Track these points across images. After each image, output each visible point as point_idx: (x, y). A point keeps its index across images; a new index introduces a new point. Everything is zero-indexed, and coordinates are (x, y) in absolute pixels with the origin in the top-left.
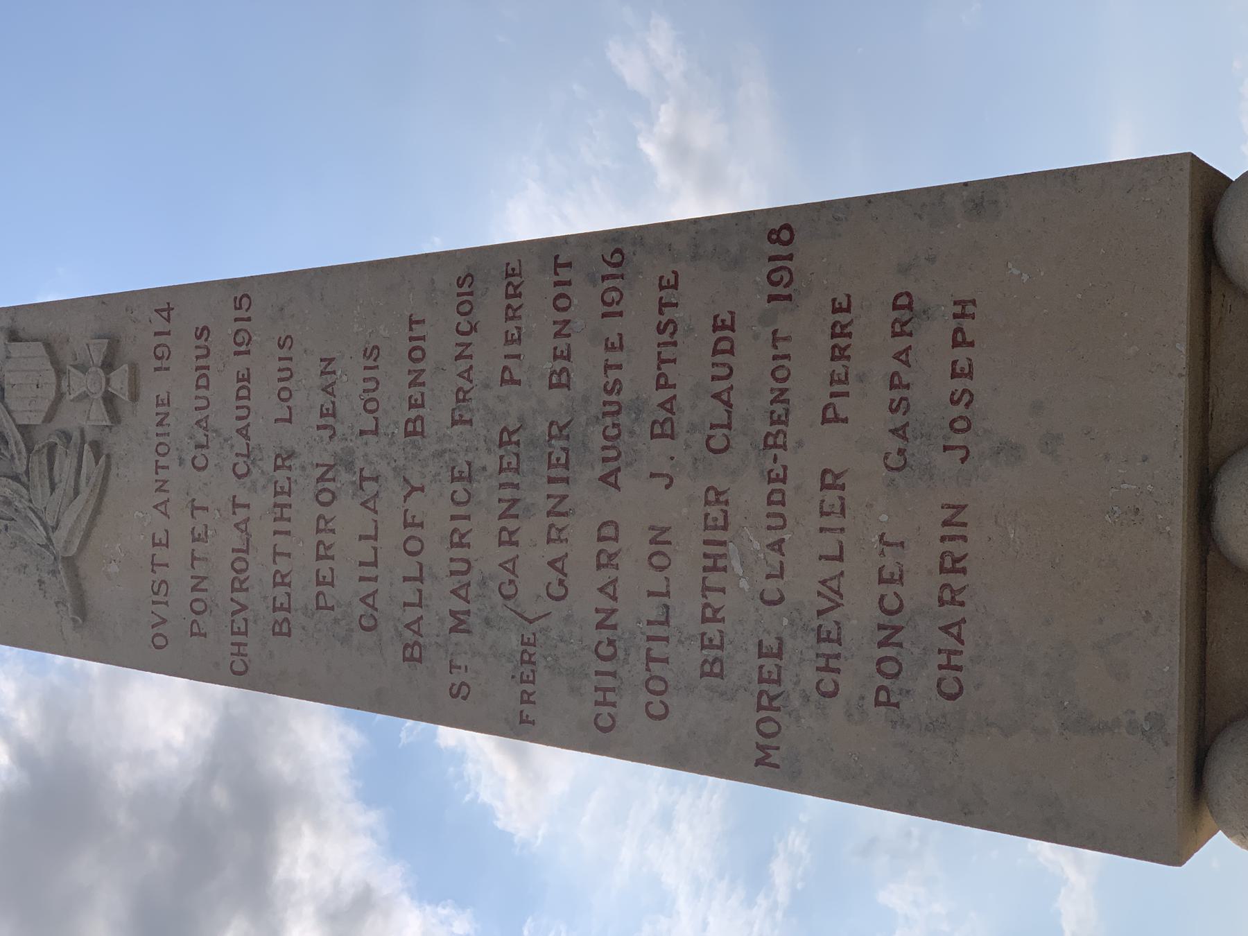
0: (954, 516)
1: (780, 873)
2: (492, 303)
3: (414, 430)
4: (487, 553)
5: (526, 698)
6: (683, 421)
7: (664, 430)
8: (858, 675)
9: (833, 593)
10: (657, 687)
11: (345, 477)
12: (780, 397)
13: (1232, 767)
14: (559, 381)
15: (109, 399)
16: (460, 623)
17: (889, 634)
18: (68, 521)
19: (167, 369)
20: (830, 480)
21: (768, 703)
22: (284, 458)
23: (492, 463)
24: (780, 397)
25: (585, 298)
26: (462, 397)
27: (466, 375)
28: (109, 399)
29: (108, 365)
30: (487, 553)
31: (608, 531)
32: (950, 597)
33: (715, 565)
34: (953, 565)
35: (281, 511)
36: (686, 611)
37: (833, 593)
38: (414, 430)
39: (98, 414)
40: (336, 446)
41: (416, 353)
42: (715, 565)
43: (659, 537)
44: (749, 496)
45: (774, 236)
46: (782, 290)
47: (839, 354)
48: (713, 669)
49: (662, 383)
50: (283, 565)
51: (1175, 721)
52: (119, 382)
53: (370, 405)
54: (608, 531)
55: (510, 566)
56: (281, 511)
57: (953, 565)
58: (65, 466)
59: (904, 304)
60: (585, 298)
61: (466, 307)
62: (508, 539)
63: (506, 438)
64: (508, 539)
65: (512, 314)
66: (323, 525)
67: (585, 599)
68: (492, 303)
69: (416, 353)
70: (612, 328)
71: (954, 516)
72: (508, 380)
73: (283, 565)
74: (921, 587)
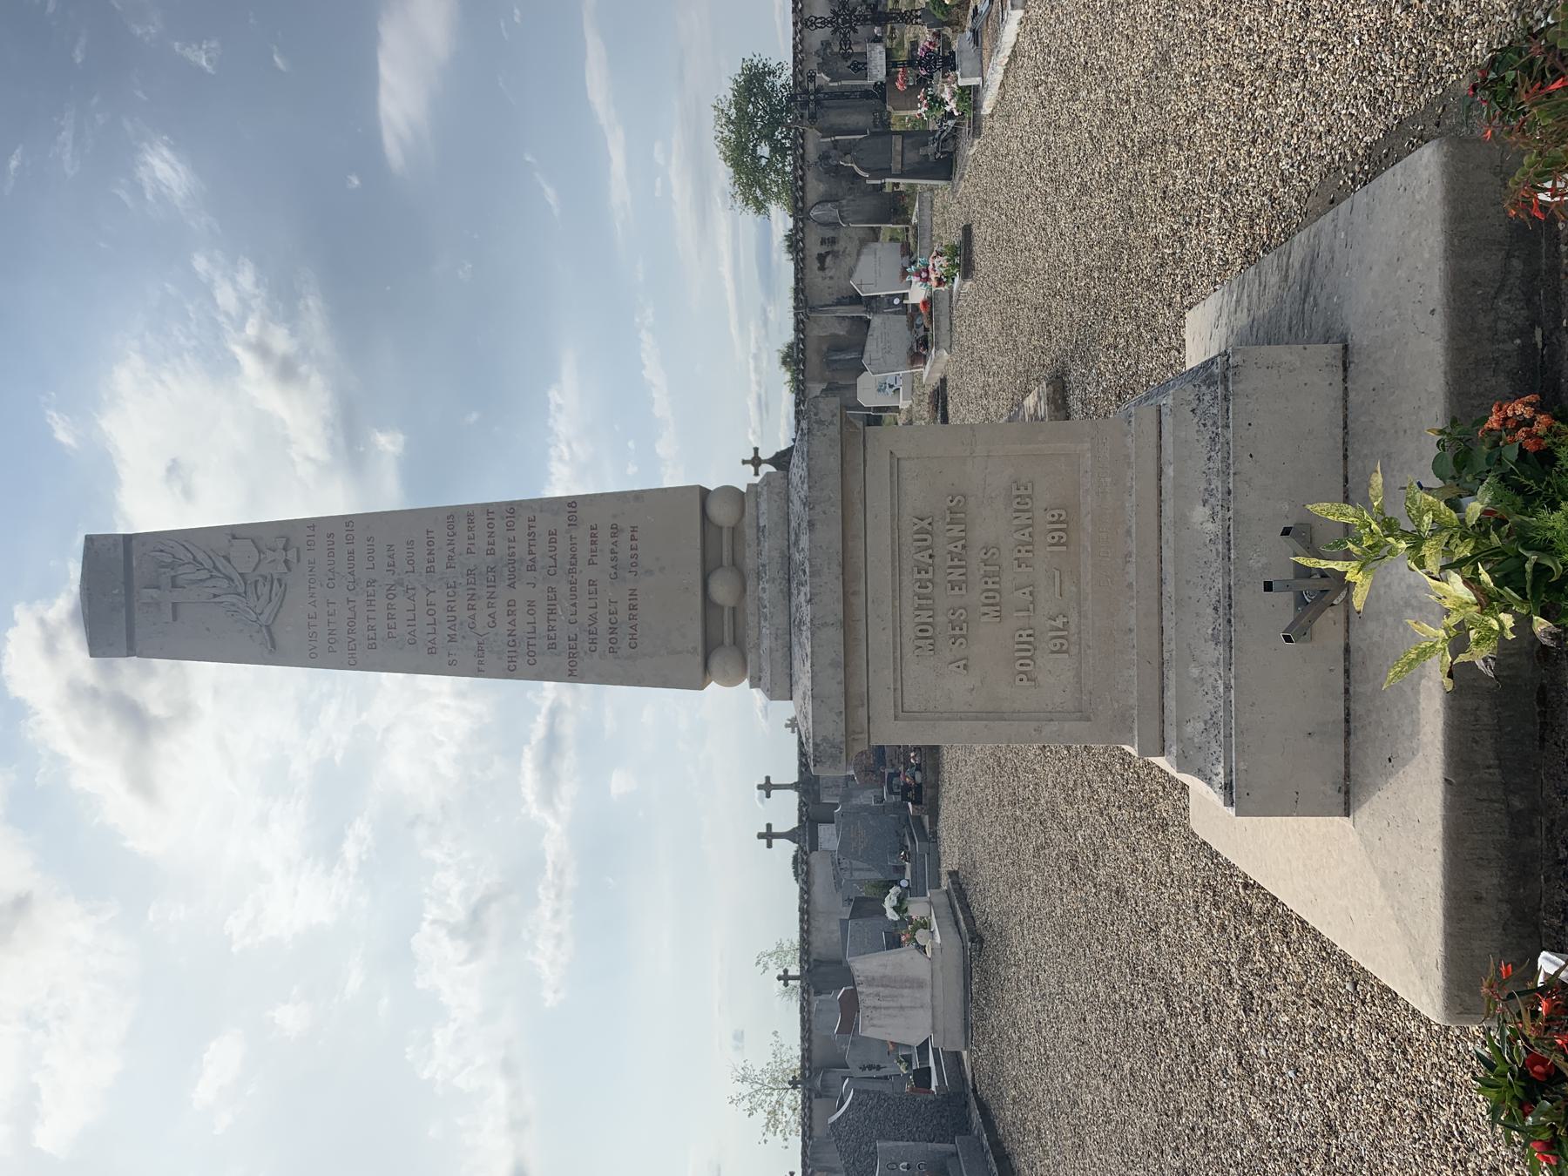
0: (633, 592)
1: (350, 850)
2: (461, 526)
3: (430, 571)
4: (463, 614)
5: (481, 663)
6: (538, 566)
7: (531, 568)
8: (603, 644)
9: (594, 619)
10: (531, 654)
11: (399, 588)
12: (574, 557)
13: (715, 663)
14: (491, 552)
15: (286, 562)
16: (452, 639)
17: (613, 631)
18: (267, 612)
19: (634, 529)
20: (592, 583)
21: (572, 656)
22: (371, 583)
23: (464, 581)
24: (574, 557)
25: (499, 525)
26: (450, 558)
27: (452, 550)
28: (286, 562)
29: (285, 549)
30: (463, 614)
31: (511, 604)
32: (633, 618)
33: (552, 612)
34: (633, 608)
35: (370, 603)
36: (542, 627)
37: (594, 619)
38: (430, 571)
39: (282, 568)
40: (396, 577)
41: (430, 543)
42: (552, 612)
43: (531, 604)
44: (563, 589)
45: (570, 505)
46: (573, 522)
47: (594, 543)
48: (552, 646)
49: (531, 553)
50: (372, 623)
51: (700, 649)
52: (292, 555)
53: (411, 561)
54: (511, 604)
55: (473, 617)
56: (370, 603)
57: (633, 608)
58: (263, 590)
59: (614, 527)
60: (499, 525)
61: (451, 526)
62: (471, 608)
63: (470, 572)
64: (471, 608)
65: (470, 529)
66: (390, 607)
67: (503, 627)
68: (461, 526)
69: (430, 543)
70: (511, 534)
71: (633, 592)
72: (469, 552)
73: (372, 623)
74: (623, 615)
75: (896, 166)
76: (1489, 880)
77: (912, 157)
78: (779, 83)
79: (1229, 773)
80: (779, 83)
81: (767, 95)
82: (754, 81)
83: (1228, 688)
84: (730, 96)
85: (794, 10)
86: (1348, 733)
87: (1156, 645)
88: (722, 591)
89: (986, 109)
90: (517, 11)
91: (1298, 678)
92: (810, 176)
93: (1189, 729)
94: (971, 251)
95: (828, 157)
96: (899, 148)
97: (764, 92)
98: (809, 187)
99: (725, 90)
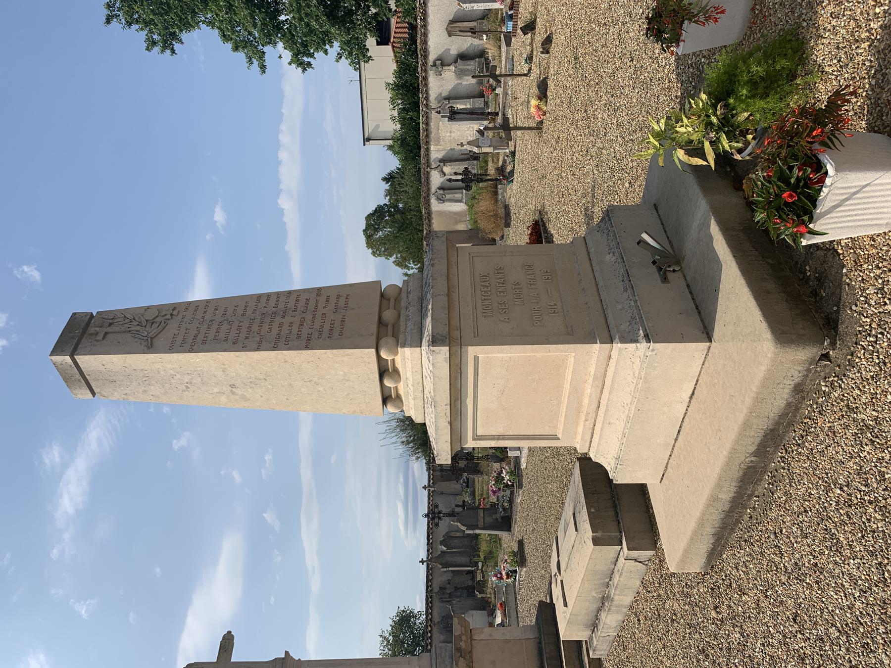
0: (344, 317)
9: (322, 327)
67: (275, 331)
71: (344, 317)
75: (481, 524)
76: (771, 285)
77: (489, 520)
78: (418, 622)
79: (645, 331)
80: (418, 622)
81: (411, 628)
82: (404, 620)
83: (636, 302)
84: (390, 628)
85: (428, 544)
86: (699, 313)
87: (600, 306)
88: (388, 383)
89: (523, 466)
90: (272, 598)
91: (665, 297)
92: (435, 630)
93: (622, 327)
94: (524, 552)
95: (445, 588)
96: (482, 515)
97: (410, 627)
98: (434, 637)
99: (387, 626)
